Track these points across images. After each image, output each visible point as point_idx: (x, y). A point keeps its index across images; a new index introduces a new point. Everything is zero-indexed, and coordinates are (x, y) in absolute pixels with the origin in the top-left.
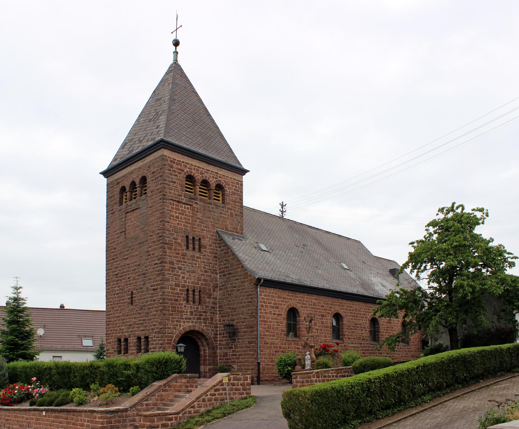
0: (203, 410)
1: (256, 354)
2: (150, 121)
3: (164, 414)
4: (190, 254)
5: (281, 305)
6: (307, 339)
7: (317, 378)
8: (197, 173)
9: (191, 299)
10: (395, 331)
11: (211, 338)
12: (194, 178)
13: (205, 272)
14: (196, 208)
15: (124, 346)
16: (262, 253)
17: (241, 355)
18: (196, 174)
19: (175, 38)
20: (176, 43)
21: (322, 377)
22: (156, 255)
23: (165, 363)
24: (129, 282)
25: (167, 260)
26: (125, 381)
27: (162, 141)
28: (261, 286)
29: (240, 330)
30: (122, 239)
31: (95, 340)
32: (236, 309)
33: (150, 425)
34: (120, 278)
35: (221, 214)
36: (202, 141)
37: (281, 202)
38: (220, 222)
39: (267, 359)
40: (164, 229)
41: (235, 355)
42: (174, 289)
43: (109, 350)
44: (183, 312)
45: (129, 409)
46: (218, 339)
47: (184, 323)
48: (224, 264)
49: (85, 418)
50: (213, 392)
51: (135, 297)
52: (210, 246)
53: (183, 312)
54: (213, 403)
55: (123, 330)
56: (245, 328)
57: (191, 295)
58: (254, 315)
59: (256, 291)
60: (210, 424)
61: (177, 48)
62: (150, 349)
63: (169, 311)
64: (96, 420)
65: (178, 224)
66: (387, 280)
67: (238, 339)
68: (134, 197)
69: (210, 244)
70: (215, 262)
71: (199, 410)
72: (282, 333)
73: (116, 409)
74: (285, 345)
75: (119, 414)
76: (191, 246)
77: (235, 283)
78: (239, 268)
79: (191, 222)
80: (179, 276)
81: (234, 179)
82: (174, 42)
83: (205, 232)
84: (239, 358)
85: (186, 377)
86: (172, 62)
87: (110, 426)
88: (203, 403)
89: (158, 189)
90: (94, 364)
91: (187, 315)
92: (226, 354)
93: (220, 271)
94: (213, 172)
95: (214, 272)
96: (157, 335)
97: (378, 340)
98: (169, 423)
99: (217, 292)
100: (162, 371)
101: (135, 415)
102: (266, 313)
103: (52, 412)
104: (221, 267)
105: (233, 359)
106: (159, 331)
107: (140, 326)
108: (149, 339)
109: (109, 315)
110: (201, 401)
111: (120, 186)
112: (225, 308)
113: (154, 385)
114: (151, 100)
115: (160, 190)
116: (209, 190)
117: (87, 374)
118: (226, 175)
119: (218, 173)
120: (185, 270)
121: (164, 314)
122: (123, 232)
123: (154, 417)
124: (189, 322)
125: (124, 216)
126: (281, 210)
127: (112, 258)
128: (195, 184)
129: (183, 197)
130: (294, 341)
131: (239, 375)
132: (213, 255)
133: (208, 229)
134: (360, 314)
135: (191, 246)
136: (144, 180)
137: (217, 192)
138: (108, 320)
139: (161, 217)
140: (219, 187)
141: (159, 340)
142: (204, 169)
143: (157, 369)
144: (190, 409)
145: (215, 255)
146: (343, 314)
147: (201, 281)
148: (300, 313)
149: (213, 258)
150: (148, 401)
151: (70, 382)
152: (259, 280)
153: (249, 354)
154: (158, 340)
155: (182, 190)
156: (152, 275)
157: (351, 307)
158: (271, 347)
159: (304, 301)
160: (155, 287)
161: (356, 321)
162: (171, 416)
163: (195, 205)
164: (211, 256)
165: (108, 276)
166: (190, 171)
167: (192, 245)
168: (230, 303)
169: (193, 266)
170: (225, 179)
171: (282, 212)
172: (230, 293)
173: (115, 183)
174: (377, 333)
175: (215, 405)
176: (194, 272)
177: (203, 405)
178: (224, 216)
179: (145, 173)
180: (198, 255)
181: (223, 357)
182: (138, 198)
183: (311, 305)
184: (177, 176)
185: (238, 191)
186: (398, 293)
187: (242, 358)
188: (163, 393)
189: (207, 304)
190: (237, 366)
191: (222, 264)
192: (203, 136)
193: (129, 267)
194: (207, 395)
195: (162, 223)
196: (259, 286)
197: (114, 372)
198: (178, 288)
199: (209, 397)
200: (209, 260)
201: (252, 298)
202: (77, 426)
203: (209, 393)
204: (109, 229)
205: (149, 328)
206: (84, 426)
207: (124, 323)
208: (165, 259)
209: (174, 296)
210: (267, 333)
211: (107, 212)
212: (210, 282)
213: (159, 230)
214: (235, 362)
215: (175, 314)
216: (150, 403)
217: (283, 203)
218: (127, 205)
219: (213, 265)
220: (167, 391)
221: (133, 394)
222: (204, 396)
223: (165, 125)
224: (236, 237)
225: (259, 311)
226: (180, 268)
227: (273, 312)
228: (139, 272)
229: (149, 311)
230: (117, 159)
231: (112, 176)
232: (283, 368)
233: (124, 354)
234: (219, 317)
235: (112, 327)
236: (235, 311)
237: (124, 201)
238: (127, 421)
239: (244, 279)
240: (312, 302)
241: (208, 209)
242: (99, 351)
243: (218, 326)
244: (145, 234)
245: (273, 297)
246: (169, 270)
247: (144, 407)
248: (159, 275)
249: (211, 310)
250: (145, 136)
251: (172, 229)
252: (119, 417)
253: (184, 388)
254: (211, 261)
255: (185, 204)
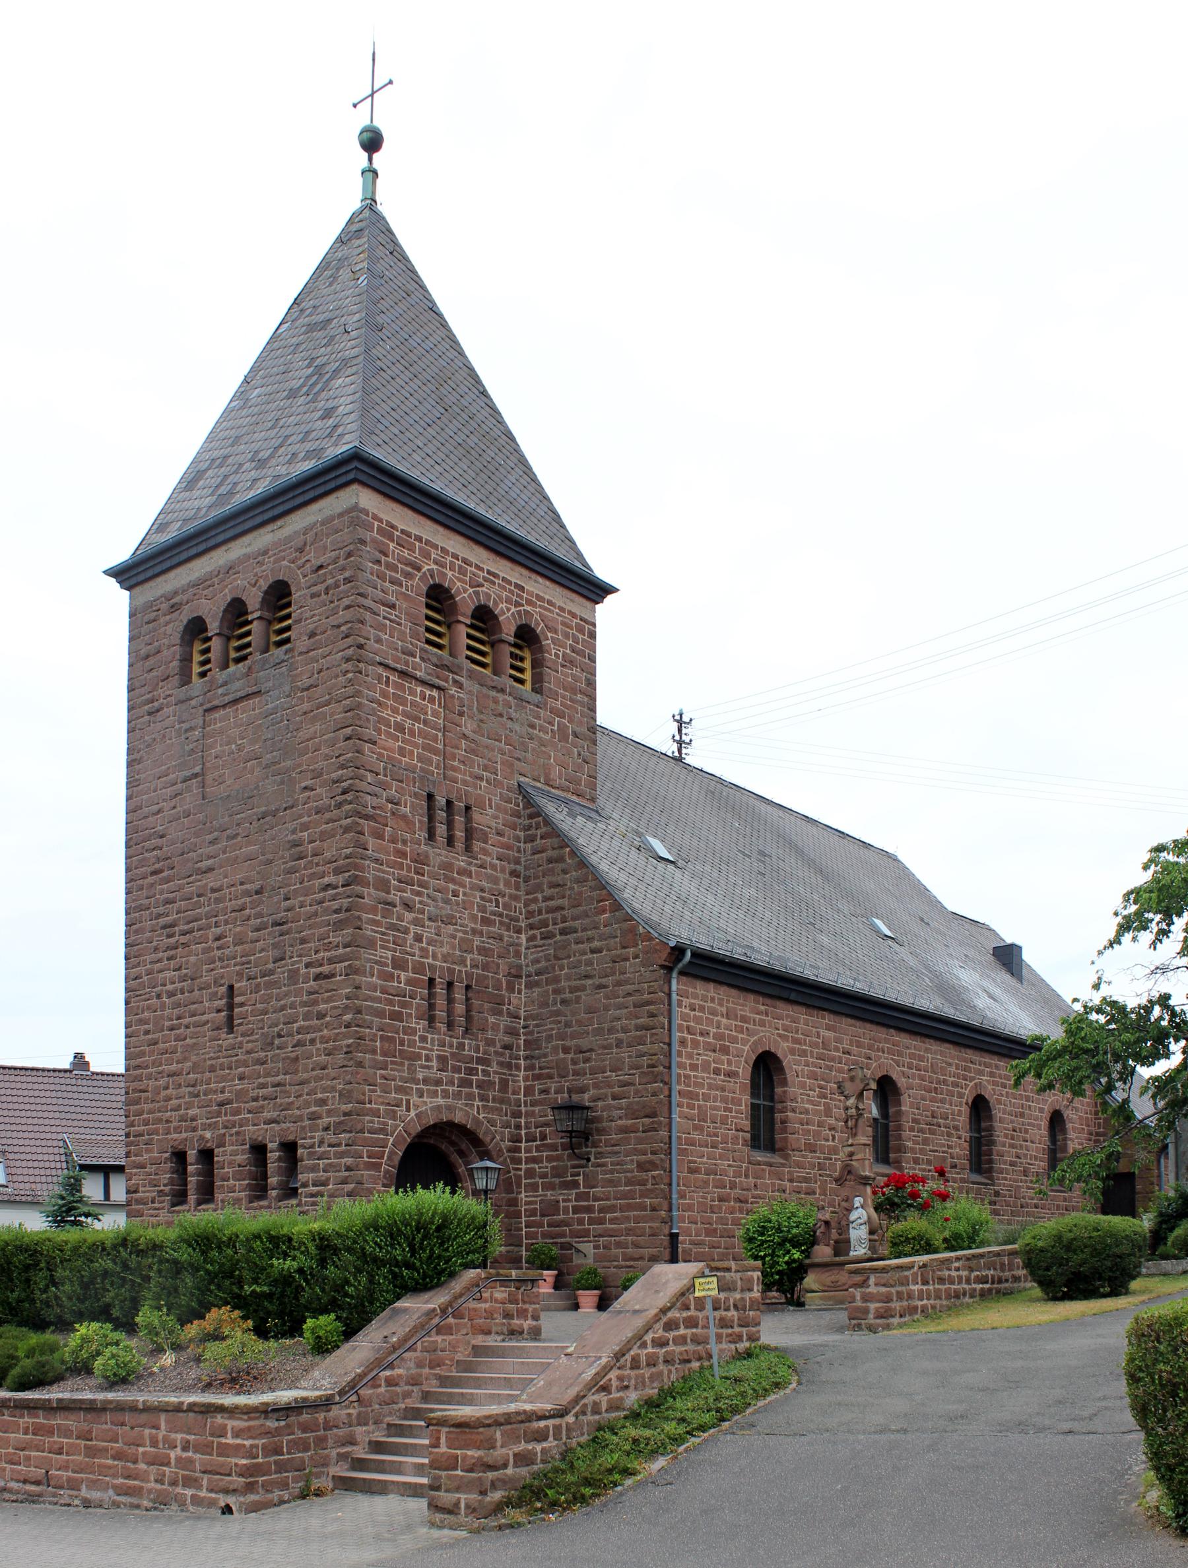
0: (632, 1398)
1: (666, 1207)
2: (293, 394)
3: (523, 1417)
4: (438, 859)
5: (734, 1040)
6: (851, 1154)
7: (923, 1284)
8: (460, 580)
9: (441, 1014)
10: (1032, 1142)
11: (501, 1150)
12: (452, 597)
13: (486, 921)
14: (456, 702)
15: (199, 1175)
16: (661, 866)
17: (612, 1209)
18: (459, 584)
19: (368, 122)
20: (372, 142)
21: (934, 1284)
22: (327, 855)
23: (438, 1229)
24: (218, 953)
25: (370, 875)
26: (269, 1296)
27: (356, 457)
28: (681, 973)
29: (604, 1124)
30: (190, 800)
31: (12, 1164)
32: (591, 1050)
33: (480, 1458)
34: (183, 939)
35: (533, 726)
36: (473, 475)
37: (676, 713)
38: (529, 755)
39: (696, 1223)
40: (359, 765)
41: (589, 1209)
42: (390, 977)
43: (136, 1192)
44: (418, 1057)
45: (337, 1398)
46: (523, 1155)
47: (421, 1096)
48: (546, 899)
49: (173, 1436)
50: (661, 1333)
51: (242, 1005)
52: (498, 834)
53: (418, 1057)
54: (661, 1373)
55: (193, 1119)
56: (627, 1117)
57: (441, 1002)
58: (662, 1073)
59: (666, 990)
60: (686, 1450)
61: (375, 156)
62: (305, 1185)
63: (374, 1052)
64: (223, 1440)
65: (402, 751)
66: (994, 980)
67: (599, 1155)
68: (233, 655)
69: (500, 826)
70: (513, 891)
71: (621, 1399)
72: (737, 1138)
73: (296, 1400)
74: (747, 1176)
75: (305, 1417)
76: (441, 829)
77: (589, 963)
78: (604, 911)
79: (441, 747)
80: (406, 931)
81: (570, 613)
82: (366, 135)
83: (484, 784)
84: (601, 1221)
85: (505, 1282)
86: (356, 204)
87: (276, 1462)
88: (633, 1373)
89: (339, 626)
90: (134, 1236)
91: (428, 1067)
92: (551, 1208)
93: (530, 921)
94: (510, 583)
95: (511, 924)
96: (330, 1137)
97: (990, 1170)
98: (538, 1447)
99: (520, 992)
100: (430, 1257)
101: (355, 1422)
102: (694, 1067)
103: (18, 1412)
104: (533, 907)
105: (581, 1222)
106: (341, 1123)
107: (262, 1107)
108: (300, 1151)
109: (138, 1067)
110: (629, 1365)
111: (185, 616)
112: (547, 1047)
113: (406, 1310)
114: (289, 329)
115: (343, 628)
116: (492, 645)
117: (106, 1273)
118: (547, 597)
119: (522, 588)
120: (423, 913)
121: (360, 1064)
122: (196, 775)
123: (493, 1429)
124: (434, 1094)
125: (200, 721)
126: (677, 738)
127: (150, 869)
128: (453, 619)
129: (418, 660)
130: (770, 1165)
131: (728, 1270)
132: (509, 867)
133: (493, 776)
134: (945, 1081)
135: (441, 829)
136: (279, 595)
137: (518, 652)
138: (133, 1085)
139: (349, 722)
140: (527, 636)
141: (341, 1155)
142: (482, 569)
143: (413, 1251)
144: (596, 1397)
145: (513, 866)
146: (901, 1082)
147: (471, 952)
148: (787, 1071)
149: (507, 876)
150: (393, 1369)
151: (33, 1301)
152: (679, 951)
153: (643, 1207)
154: (336, 1153)
155: (414, 635)
156: (310, 927)
157: (921, 1059)
158: (706, 1183)
159: (797, 1032)
160: (325, 969)
161: (934, 1106)
162: (542, 1424)
163: (453, 691)
164: (503, 871)
165: (137, 932)
166: (439, 571)
167: (444, 827)
168: (569, 1030)
169: (447, 901)
170: (545, 609)
171: (680, 743)
172: (567, 995)
173: (165, 606)
174: (984, 1148)
175: (666, 1380)
176: (449, 920)
177: (633, 1382)
178: (541, 734)
179: (284, 570)
180: (461, 862)
181: (542, 1215)
182: (258, 656)
183: (816, 1045)
184: (401, 585)
185: (581, 653)
186: (1099, 1011)
187: (612, 1221)
188: (439, 1338)
189: (490, 1035)
190: (595, 1247)
191: (540, 896)
192: (473, 460)
193: (217, 901)
194: (644, 1345)
195: (355, 744)
196: (675, 974)
197: (222, 1265)
198: (403, 975)
199: (650, 1350)
200: (495, 881)
201: (652, 1015)
202: (135, 1462)
203: (648, 1338)
204: (137, 767)
205: (297, 1112)
206: (168, 1464)
207: (197, 1096)
208: (362, 869)
209: (391, 1003)
210: (696, 1136)
211: (130, 709)
212: (499, 957)
213: (342, 767)
214: (586, 1233)
215: (393, 1063)
216: (400, 1376)
217: (681, 715)
218: (212, 682)
219: (507, 898)
220: (449, 1330)
221: (322, 1348)
222: (635, 1347)
223: (357, 405)
224: (577, 809)
225: (675, 1059)
226: (408, 906)
227: (713, 1065)
228: (260, 915)
229: (299, 1051)
230: (168, 524)
231: (152, 584)
232: (774, 1252)
233: (199, 1203)
234: (526, 1079)
235: (150, 1112)
236: (586, 1060)
237: (196, 669)
238: (330, 1442)
239: (624, 948)
240: (818, 1037)
241: (492, 706)
242: (63, 1198)
243: (523, 1109)
244: (282, 783)
245: (714, 1012)
246: (374, 910)
247: (382, 1389)
248: (339, 926)
249: (502, 1055)
250: (280, 446)
251: (385, 769)
252: (305, 1428)
253: (499, 1320)
254: (502, 886)
255: (423, 683)
